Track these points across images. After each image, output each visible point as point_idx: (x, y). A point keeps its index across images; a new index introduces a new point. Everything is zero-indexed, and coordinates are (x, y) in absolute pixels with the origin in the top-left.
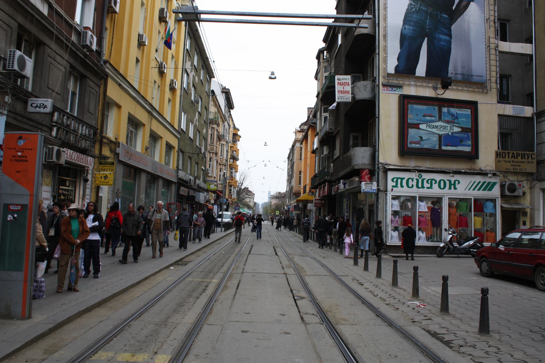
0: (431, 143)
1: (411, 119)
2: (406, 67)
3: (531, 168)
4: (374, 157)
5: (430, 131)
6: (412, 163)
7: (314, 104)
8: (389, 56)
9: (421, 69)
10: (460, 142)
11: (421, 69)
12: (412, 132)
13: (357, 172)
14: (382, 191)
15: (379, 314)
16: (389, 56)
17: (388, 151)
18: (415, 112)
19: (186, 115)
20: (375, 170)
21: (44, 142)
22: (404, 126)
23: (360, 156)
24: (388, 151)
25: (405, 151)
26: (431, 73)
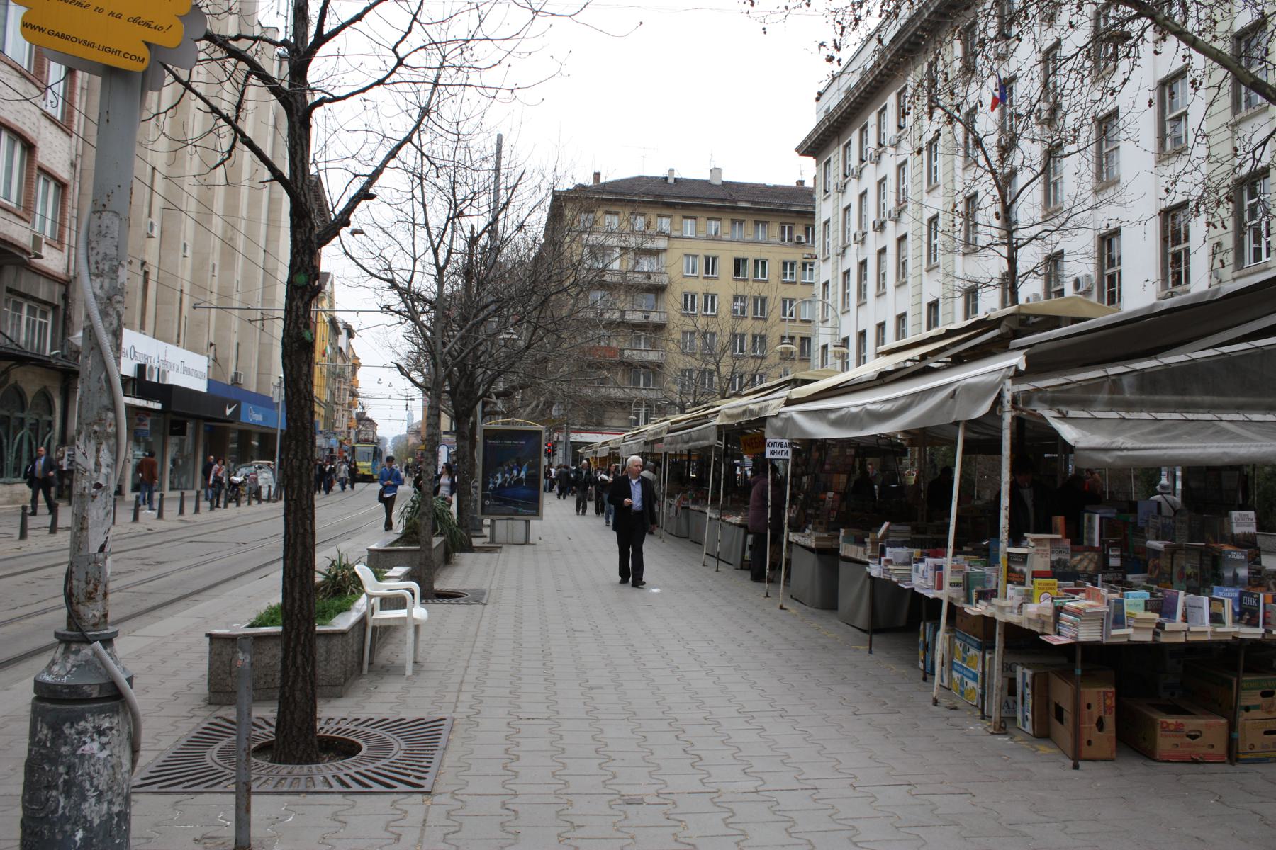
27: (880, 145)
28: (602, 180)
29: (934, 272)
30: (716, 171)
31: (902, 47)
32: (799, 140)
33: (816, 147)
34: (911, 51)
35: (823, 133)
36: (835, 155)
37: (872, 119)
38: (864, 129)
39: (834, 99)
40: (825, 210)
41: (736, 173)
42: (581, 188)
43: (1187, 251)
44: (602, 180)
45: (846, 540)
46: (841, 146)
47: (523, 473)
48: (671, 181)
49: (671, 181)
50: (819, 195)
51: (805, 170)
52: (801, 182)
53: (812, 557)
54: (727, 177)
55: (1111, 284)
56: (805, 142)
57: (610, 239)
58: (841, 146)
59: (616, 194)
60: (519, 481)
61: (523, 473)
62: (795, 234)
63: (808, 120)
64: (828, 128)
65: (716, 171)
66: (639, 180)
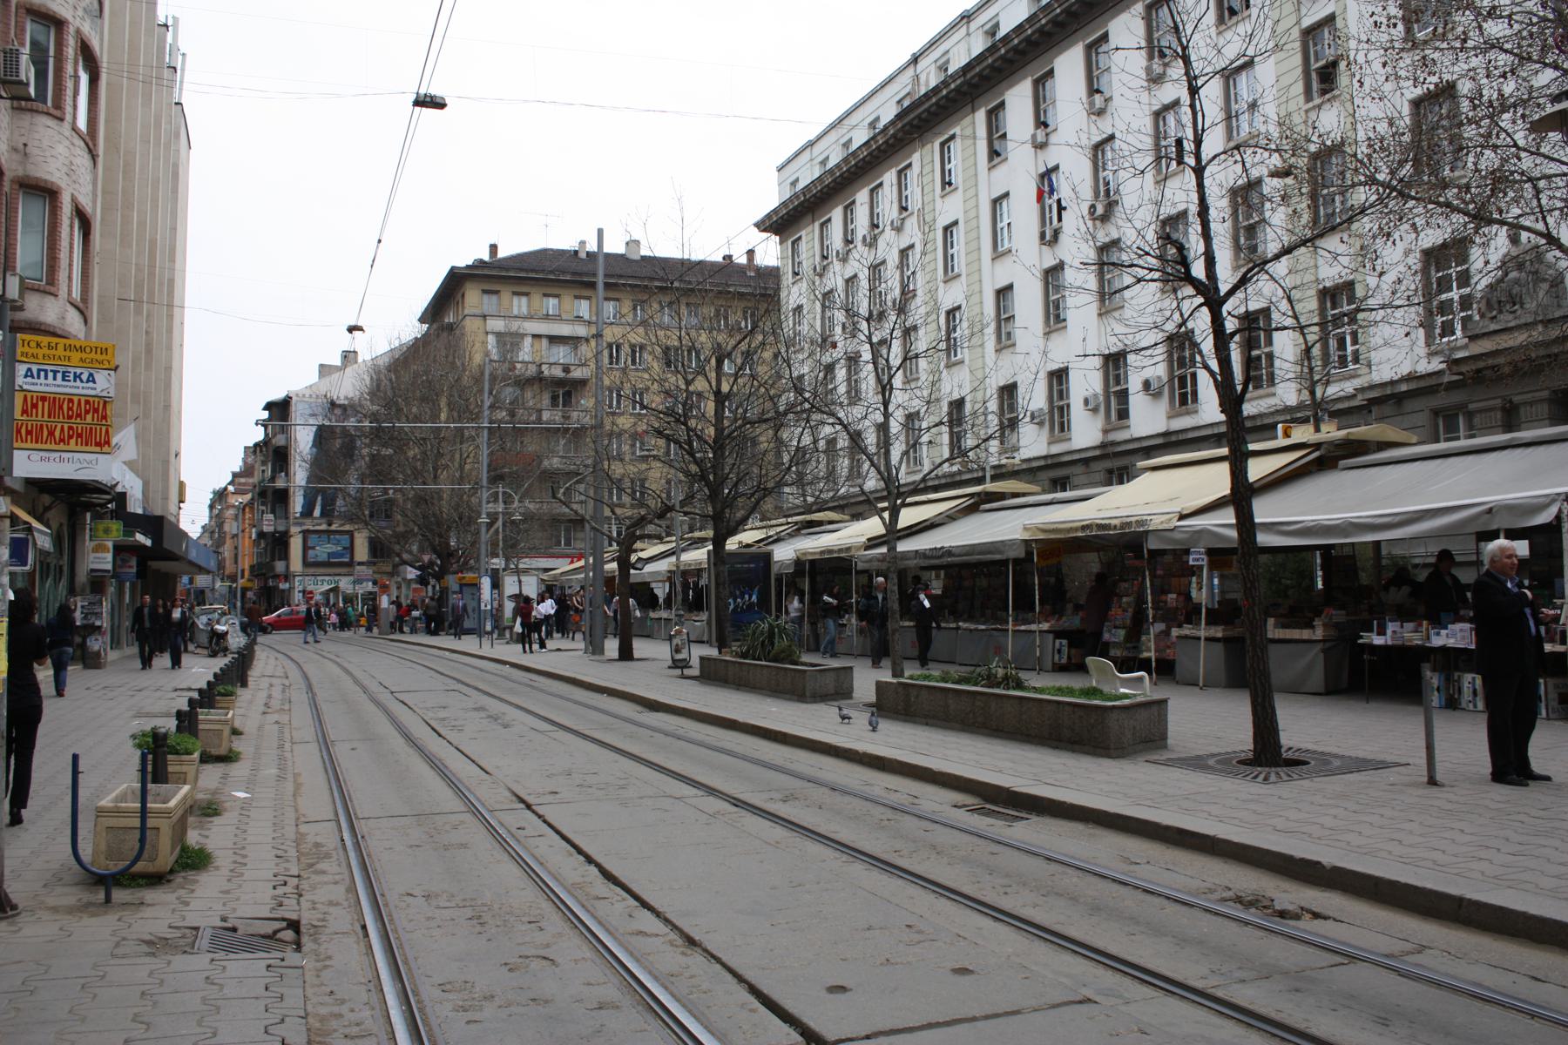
0: (323, 558)
1: (310, 544)
2: (307, 512)
3: (389, 569)
4: (288, 567)
5: (322, 551)
6: (311, 570)
7: (1228, 485)
8: (297, 504)
9: (317, 513)
10: (342, 556)
11: (317, 513)
12: (311, 553)
13: (276, 576)
14: (291, 588)
15: (737, 803)
16: (297, 504)
17: (296, 564)
18: (312, 540)
19: (638, 545)
20: (287, 577)
21: (459, 631)
22: (306, 548)
23: (280, 566)
24: (296, 564)
25: (306, 564)
26: (323, 514)
27: (874, 226)
28: (501, 254)
29: (955, 369)
30: (633, 243)
31: (910, 123)
32: (760, 214)
33: (782, 223)
34: (918, 127)
35: (795, 208)
36: (809, 236)
37: (862, 196)
38: (849, 208)
39: (808, 174)
40: (794, 294)
41: (663, 244)
42: (480, 264)
43: (1270, 356)
44: (501, 254)
45: (1276, 626)
46: (817, 225)
47: (754, 598)
48: (583, 255)
49: (583, 255)
50: (787, 279)
51: (770, 252)
52: (728, 258)
53: (1219, 647)
54: (645, 252)
55: (1183, 384)
56: (769, 216)
57: (488, 323)
58: (817, 225)
59: (526, 271)
60: (751, 605)
61: (754, 598)
62: (732, 320)
63: (770, 198)
64: (801, 204)
65: (633, 243)
66: (543, 253)
